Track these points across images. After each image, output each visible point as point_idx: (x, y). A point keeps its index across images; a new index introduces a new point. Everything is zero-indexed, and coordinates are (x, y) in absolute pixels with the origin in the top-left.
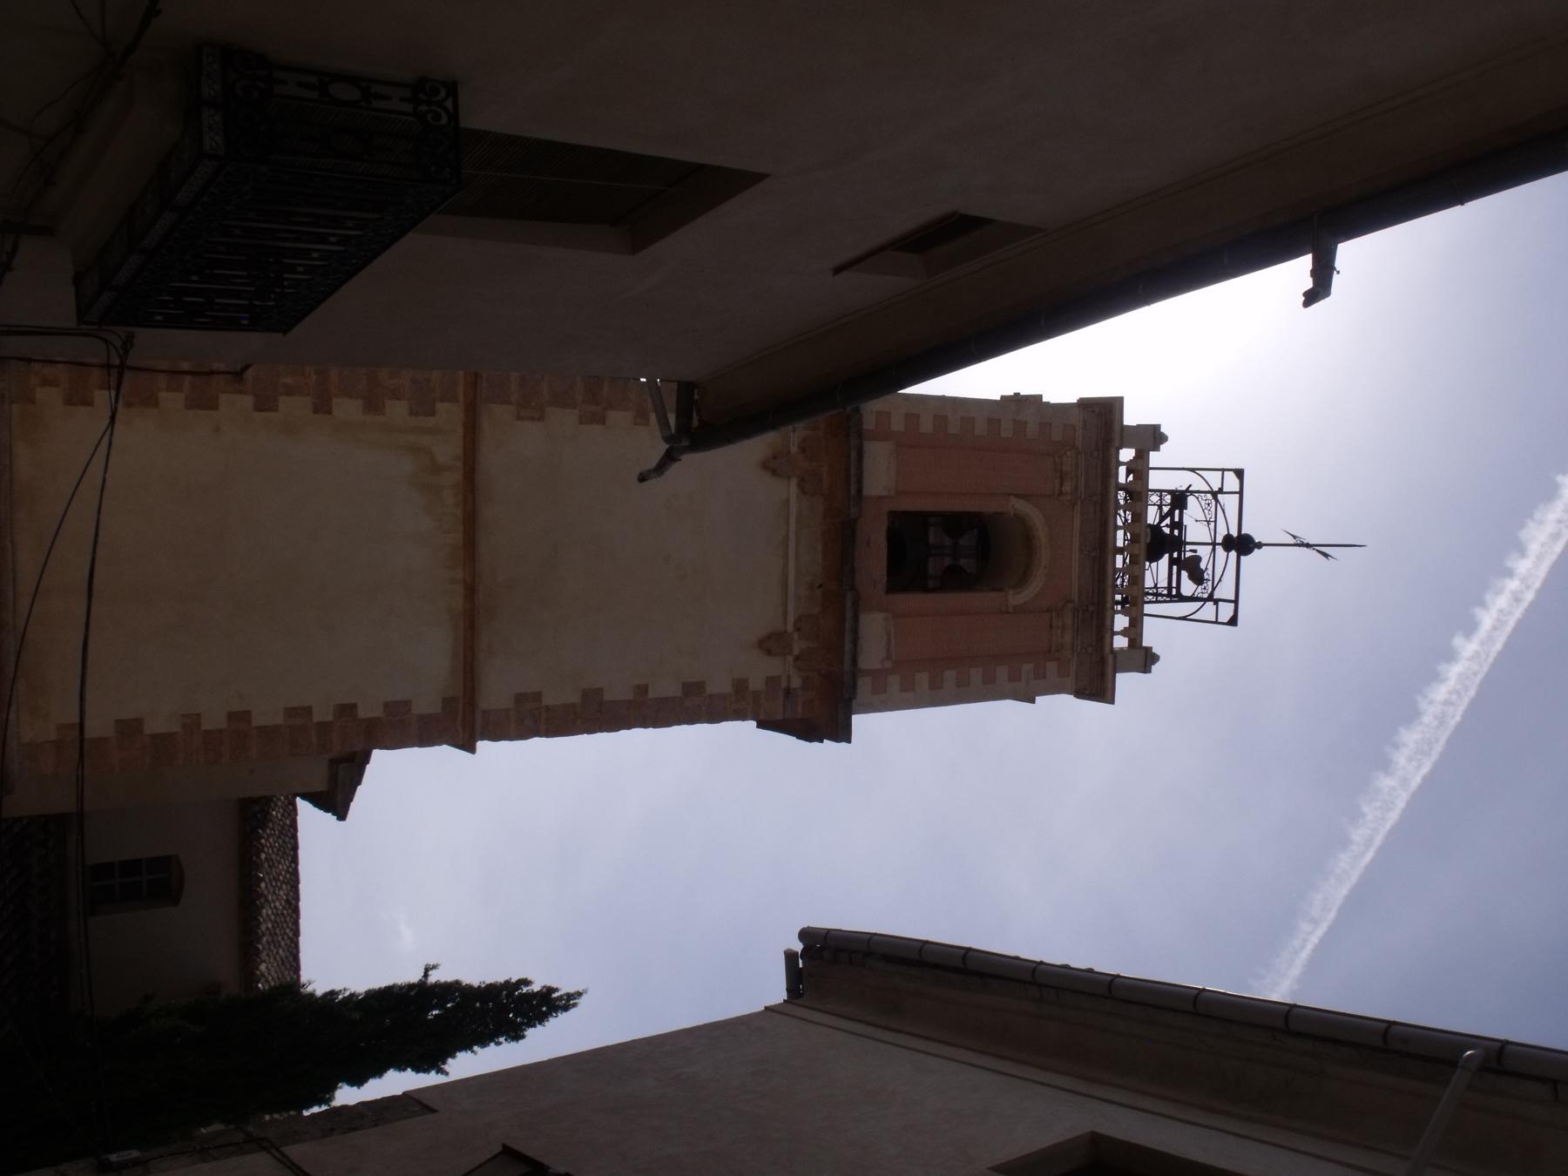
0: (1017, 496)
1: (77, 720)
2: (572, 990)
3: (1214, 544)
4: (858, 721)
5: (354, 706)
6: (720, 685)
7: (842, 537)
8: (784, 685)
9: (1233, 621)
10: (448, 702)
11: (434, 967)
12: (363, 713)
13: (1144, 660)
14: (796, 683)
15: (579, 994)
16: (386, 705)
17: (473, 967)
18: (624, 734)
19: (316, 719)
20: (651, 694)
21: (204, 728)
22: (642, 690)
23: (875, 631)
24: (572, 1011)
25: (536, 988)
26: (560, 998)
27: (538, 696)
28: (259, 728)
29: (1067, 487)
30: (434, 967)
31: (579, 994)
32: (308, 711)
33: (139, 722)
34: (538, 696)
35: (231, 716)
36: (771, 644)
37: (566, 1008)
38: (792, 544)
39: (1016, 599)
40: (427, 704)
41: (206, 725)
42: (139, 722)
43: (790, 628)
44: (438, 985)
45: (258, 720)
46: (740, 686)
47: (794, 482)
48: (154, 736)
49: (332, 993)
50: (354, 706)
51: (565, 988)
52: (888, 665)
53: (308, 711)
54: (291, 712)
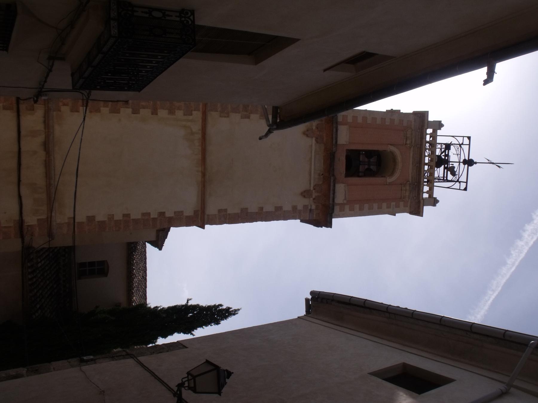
0: (391, 145)
1: (17, 217)
2: (236, 308)
3: (459, 162)
4: (206, 226)
5: (164, 213)
7: (330, 158)
8: (309, 208)
9: (465, 189)
10: (196, 212)
11: (190, 299)
12: (168, 215)
13: (434, 202)
14: (314, 207)
15: (239, 310)
16: (175, 213)
17: (204, 302)
18: (255, 223)
19: (152, 217)
20: (264, 210)
22: (261, 209)
23: (341, 190)
24: (236, 315)
27: (226, 210)
29: (408, 142)
30: (190, 299)
31: (239, 310)
32: (149, 214)
34: (226, 210)
35: (124, 215)
36: (305, 194)
37: (234, 314)
38: (313, 160)
39: (390, 180)
40: (189, 212)
41: (116, 218)
43: (312, 189)
44: (191, 305)
45: (133, 217)
47: (314, 139)
48: (99, 222)
49: (157, 307)
50: (164, 213)
51: (234, 307)
52: (345, 202)
54: (143, 214)
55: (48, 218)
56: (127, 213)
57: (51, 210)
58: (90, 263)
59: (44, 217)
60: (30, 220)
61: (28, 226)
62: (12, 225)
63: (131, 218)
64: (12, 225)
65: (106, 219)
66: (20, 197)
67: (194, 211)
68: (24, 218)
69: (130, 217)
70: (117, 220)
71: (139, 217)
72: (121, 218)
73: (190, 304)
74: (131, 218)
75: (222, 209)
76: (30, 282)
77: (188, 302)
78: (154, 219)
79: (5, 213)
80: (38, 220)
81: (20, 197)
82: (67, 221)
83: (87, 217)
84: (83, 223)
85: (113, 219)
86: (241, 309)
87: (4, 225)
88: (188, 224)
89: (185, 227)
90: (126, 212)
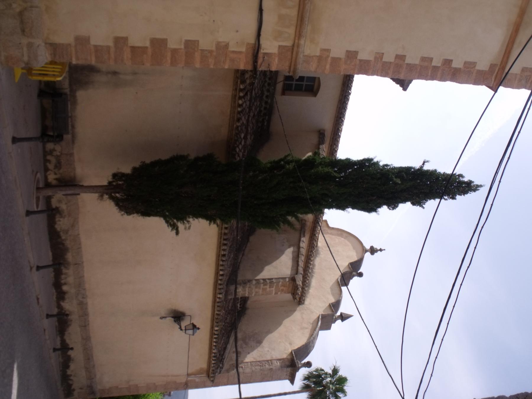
1: (252, 40)
2: (479, 184)
5: (452, 61)
6: (457, 64)
10: (492, 66)
11: (428, 162)
12: (455, 65)
15: (481, 186)
16: (465, 63)
17: (444, 168)
19: (434, 64)
21: (384, 60)
24: (477, 192)
25: (466, 179)
26: (474, 185)
28: (407, 64)
30: (428, 162)
31: (481, 186)
32: (431, 59)
33: (356, 53)
35: (398, 57)
37: (475, 190)
40: (483, 65)
41: (385, 59)
42: (356, 53)
44: (428, 171)
45: (408, 61)
46: (379, 56)
48: (361, 61)
49: (387, 165)
50: (452, 61)
51: (476, 182)
53: (431, 59)
54: (423, 59)
55: (293, 45)
56: (402, 54)
57: (299, 34)
58: (308, 78)
59: (289, 43)
60: (270, 46)
61: (265, 54)
62: (244, 50)
63: (406, 62)
64: (244, 50)
65: (372, 58)
66: (261, 10)
67: (491, 64)
68: (262, 42)
69: (404, 61)
70: (386, 62)
71: (417, 62)
72: (392, 60)
73: (425, 168)
74: (406, 62)
75: (527, 68)
76: (239, 109)
77: (423, 164)
78: (435, 67)
79: (237, 31)
80: (280, 46)
81: (261, 10)
82: (318, 54)
83: (347, 51)
84: (340, 59)
85: (382, 58)
86: (484, 186)
87: (233, 49)
88: (476, 82)
89: (471, 85)
90: (400, 52)
